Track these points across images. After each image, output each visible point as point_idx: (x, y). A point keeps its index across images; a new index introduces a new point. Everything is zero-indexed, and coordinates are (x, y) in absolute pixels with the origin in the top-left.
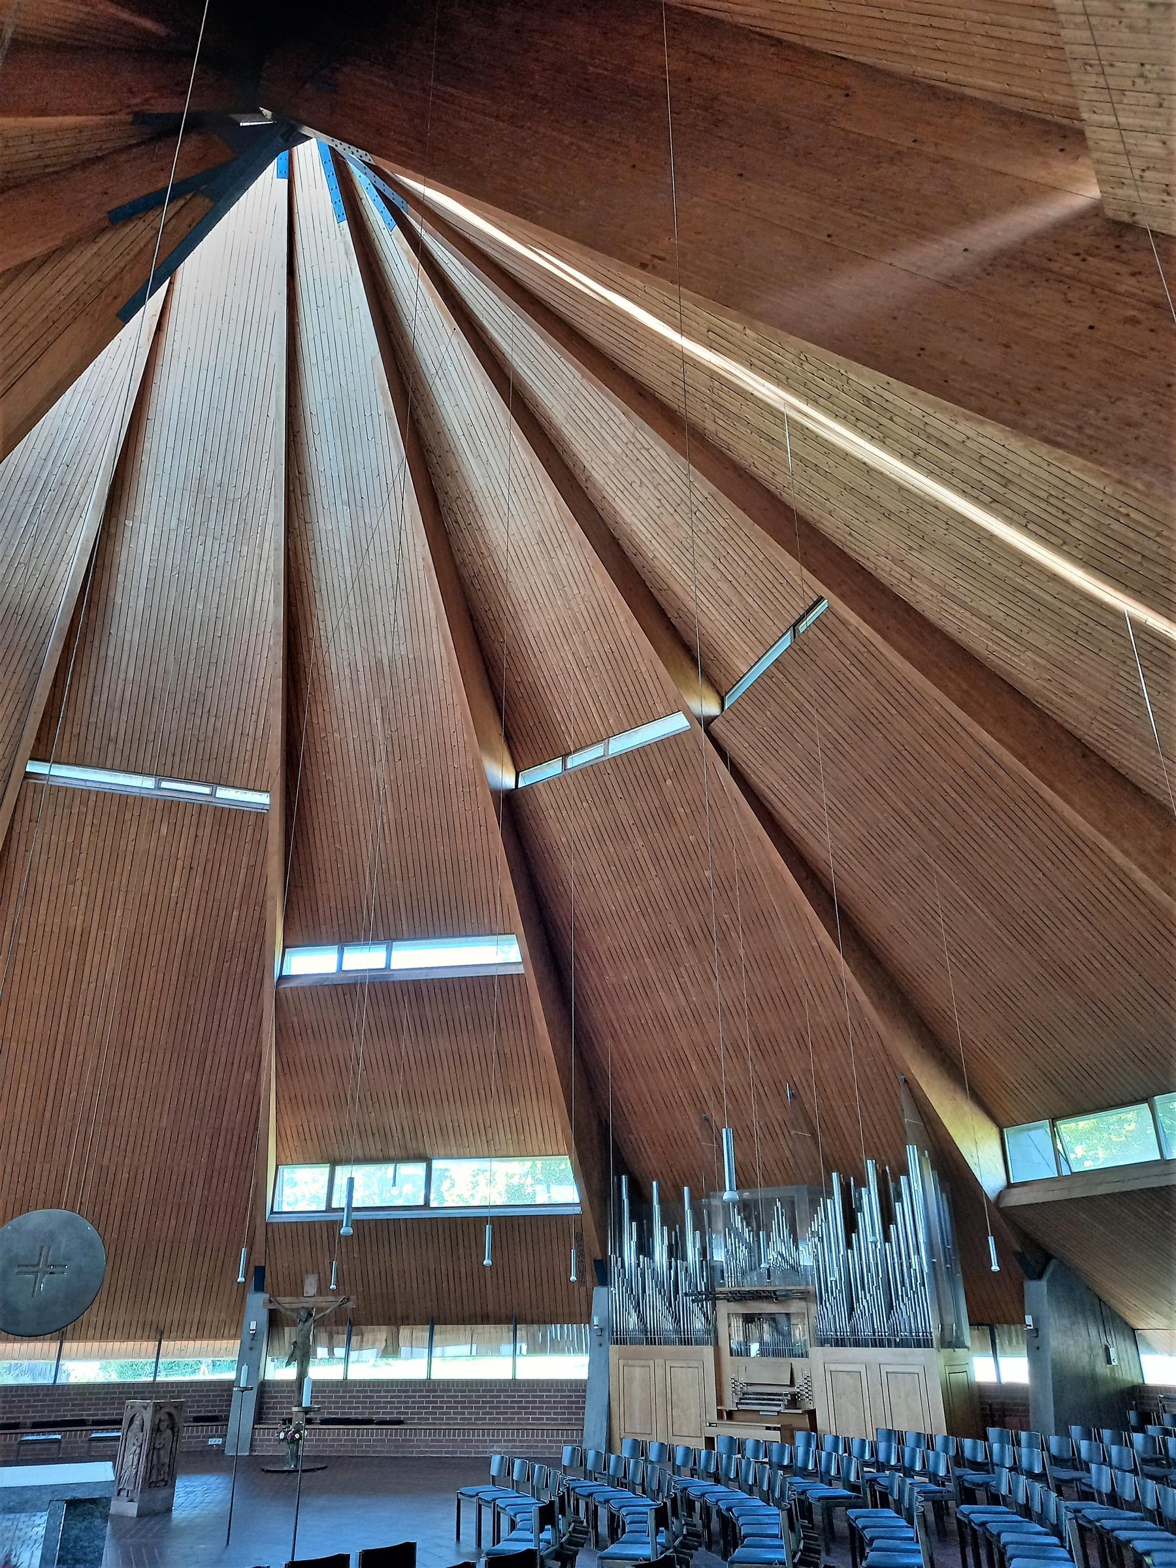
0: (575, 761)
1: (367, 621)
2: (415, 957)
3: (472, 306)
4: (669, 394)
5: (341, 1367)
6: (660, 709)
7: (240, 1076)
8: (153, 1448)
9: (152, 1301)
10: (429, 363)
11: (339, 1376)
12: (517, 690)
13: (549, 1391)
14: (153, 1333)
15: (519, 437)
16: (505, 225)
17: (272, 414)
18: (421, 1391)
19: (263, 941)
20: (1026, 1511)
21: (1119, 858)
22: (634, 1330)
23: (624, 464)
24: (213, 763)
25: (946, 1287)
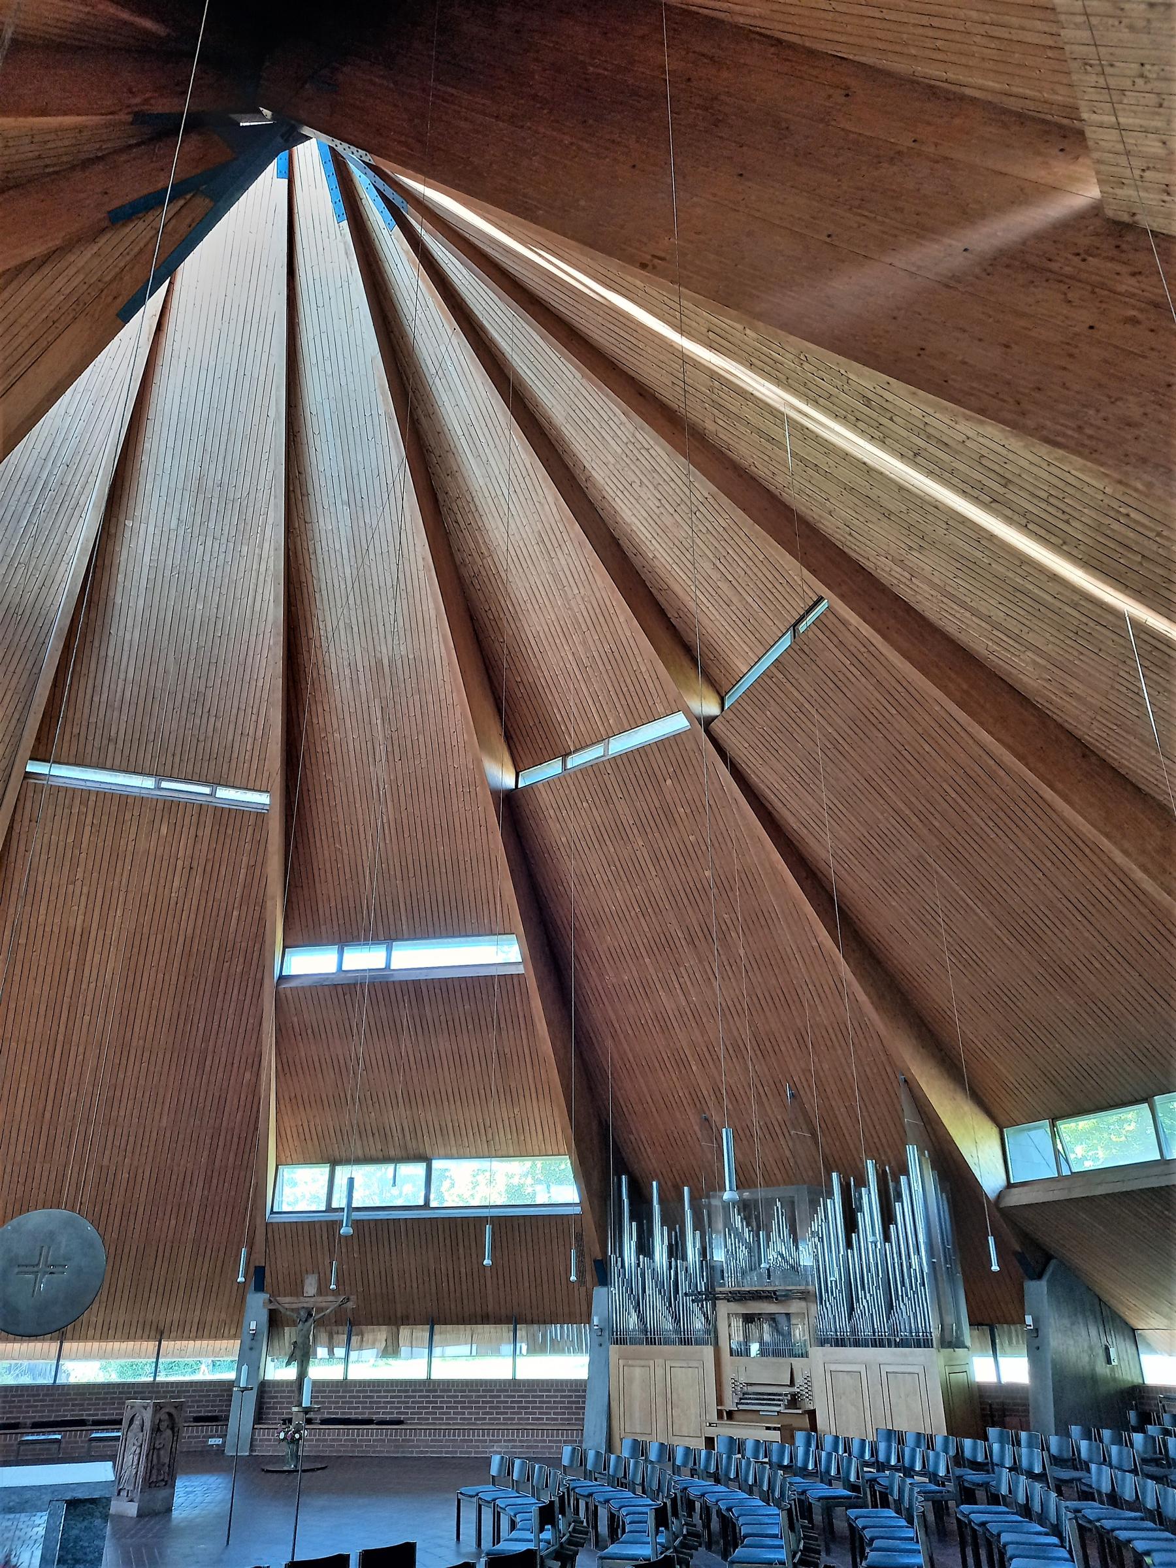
0: (575, 761)
1: (367, 621)
2: (415, 957)
3: (472, 306)
4: (669, 394)
5: (341, 1367)
6: (660, 709)
7: (240, 1076)
8: (153, 1448)
9: (152, 1301)
10: (429, 363)
11: (339, 1376)
12: (517, 690)
13: (549, 1391)
14: (153, 1333)
15: (519, 437)
16: (505, 225)
17: (272, 414)
18: (421, 1391)
19: (263, 941)
20: (1026, 1511)
21: (1119, 858)
22: (634, 1330)
23: (624, 464)
24: (213, 763)
25: (946, 1287)
